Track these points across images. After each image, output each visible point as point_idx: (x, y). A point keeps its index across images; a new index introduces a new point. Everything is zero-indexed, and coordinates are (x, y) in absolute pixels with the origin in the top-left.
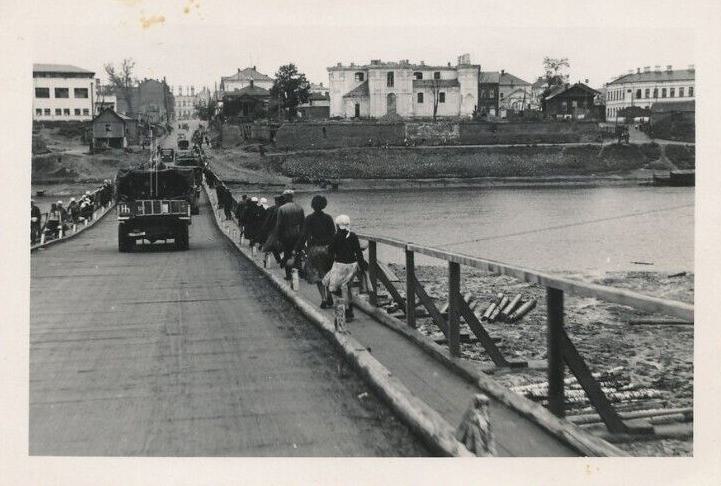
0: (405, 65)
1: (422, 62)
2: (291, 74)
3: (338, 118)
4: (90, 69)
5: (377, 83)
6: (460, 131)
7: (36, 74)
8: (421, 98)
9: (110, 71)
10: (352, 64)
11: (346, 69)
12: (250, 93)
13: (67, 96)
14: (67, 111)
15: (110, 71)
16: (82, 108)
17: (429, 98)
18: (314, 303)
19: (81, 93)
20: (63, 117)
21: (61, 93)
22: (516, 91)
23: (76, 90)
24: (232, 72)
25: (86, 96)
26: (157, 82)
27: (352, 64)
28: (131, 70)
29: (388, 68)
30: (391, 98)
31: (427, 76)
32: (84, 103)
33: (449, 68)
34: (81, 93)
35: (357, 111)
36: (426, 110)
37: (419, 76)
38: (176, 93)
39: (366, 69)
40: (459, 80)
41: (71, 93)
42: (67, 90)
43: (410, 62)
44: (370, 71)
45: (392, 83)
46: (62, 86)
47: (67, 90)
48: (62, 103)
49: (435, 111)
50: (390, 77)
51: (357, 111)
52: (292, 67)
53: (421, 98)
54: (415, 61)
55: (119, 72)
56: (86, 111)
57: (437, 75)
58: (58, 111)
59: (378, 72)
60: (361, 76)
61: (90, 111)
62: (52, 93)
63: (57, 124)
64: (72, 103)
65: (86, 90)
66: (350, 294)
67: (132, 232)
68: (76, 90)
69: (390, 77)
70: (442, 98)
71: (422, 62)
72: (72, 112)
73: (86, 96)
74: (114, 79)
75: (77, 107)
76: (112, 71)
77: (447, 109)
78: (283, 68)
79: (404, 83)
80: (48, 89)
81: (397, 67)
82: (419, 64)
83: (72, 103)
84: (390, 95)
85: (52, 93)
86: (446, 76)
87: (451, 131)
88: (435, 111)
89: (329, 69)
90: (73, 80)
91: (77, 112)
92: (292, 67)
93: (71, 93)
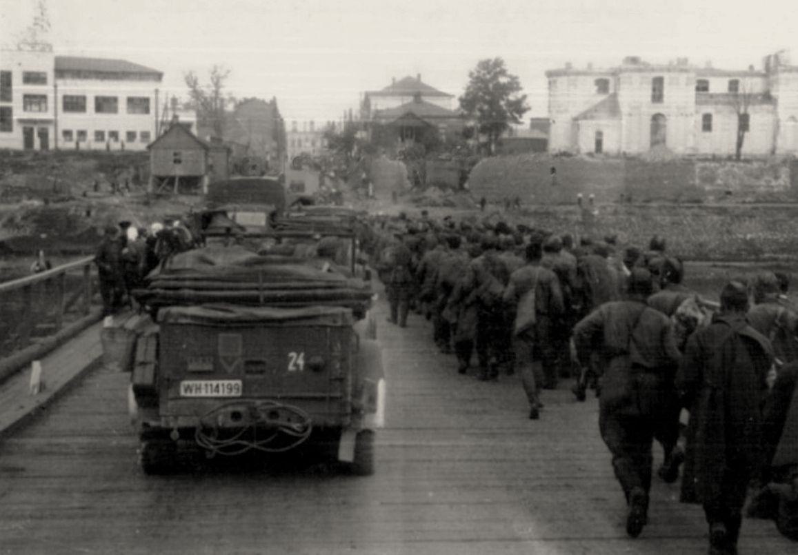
0: (681, 67)
3: (565, 154)
4: (158, 68)
5: (634, 94)
7: (46, 31)
8: (707, 124)
9: (192, 82)
10: (590, 66)
11: (578, 74)
14: (114, 135)
15: (192, 82)
16: (138, 130)
17: (725, 124)
18: (71, 270)
19: (139, 105)
21: (105, 104)
24: (380, 83)
25: (147, 111)
26: (263, 102)
27: (590, 66)
28: (223, 82)
29: (653, 70)
31: (718, 86)
33: (751, 73)
34: (139, 105)
35: (599, 143)
36: (722, 139)
37: (702, 87)
38: (288, 127)
39: (615, 73)
40: (773, 93)
41: (122, 105)
42: (115, 100)
44: (623, 76)
46: (107, 94)
47: (115, 100)
48: (106, 122)
49: (740, 144)
50: (658, 85)
51: (599, 143)
53: (707, 124)
54: (697, 59)
57: (734, 85)
58: (100, 135)
59: (636, 77)
60: (602, 85)
62: (91, 105)
65: (146, 100)
67: (780, 359)
69: (658, 85)
73: (147, 111)
74: (196, 94)
75: (131, 129)
76: (195, 83)
78: (485, 65)
79: (680, 95)
80: (84, 98)
81: (669, 69)
82: (702, 66)
83: (123, 121)
85: (91, 105)
86: (752, 86)
87: (777, 178)
88: (740, 144)
89: (551, 75)
92: (498, 63)
93: (122, 105)
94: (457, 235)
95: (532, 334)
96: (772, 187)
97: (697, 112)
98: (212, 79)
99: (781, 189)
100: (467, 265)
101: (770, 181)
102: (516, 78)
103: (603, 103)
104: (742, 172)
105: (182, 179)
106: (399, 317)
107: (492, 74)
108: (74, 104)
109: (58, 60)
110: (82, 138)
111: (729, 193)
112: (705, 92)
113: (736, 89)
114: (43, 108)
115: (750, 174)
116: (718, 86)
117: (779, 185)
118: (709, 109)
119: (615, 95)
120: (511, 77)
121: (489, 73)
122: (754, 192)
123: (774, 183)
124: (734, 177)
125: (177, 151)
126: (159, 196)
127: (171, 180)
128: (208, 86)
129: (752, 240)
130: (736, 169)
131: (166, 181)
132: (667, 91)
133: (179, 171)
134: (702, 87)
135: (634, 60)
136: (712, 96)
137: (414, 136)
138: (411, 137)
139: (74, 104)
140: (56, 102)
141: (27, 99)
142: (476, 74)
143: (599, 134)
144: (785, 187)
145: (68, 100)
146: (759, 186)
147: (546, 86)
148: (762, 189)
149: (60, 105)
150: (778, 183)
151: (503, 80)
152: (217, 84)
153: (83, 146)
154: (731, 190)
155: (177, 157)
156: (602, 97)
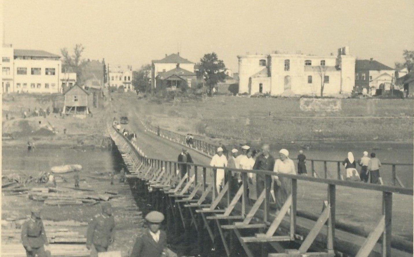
1: (214, 166)
2: (213, 61)
6: (343, 105)
12: (177, 73)
13: (40, 74)
17: (317, 80)
20: (36, 90)
22: (382, 75)
23: (25, 73)
25: (54, 74)
30: (287, 79)
32: (51, 79)
35: (261, 88)
36: (314, 89)
43: (181, 55)
45: (288, 68)
51: (261, 88)
52: (214, 55)
55: (71, 54)
56: (53, 85)
58: (33, 85)
61: (57, 85)
63: (34, 95)
64: (42, 78)
66: (265, 223)
68: (25, 73)
70: (327, 79)
71: (214, 166)
72: (43, 86)
76: (67, 54)
77: (331, 89)
78: (207, 56)
84: (286, 77)
87: (335, 105)
90: (45, 60)
91: (47, 86)
92: (214, 55)
96: (334, 109)
98: (75, 52)
100: (325, 196)
101: (333, 107)
104: (320, 103)
105: (77, 107)
107: (211, 60)
108: (21, 71)
109: (15, 51)
110: (25, 86)
112: (310, 66)
113: (324, 64)
114: (8, 73)
115: (324, 104)
116: (315, 62)
117: (336, 109)
120: (220, 61)
121: (209, 59)
122: (326, 112)
123: (334, 108)
125: (76, 96)
126: (67, 115)
127: (73, 108)
128: (74, 57)
130: (317, 102)
131: (71, 109)
133: (77, 104)
137: (176, 85)
138: (175, 85)
139: (21, 71)
140: (14, 71)
141: (4, 69)
143: (261, 85)
145: (19, 69)
146: (328, 109)
148: (329, 110)
149: (16, 72)
150: (336, 108)
151: (216, 63)
152: (78, 55)
153: (25, 90)
155: (76, 98)
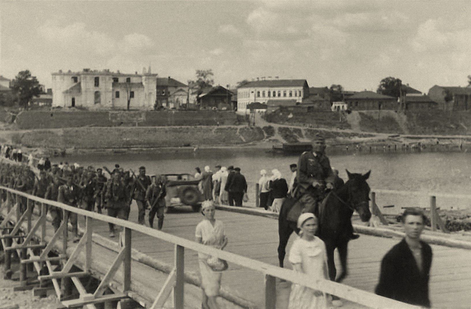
0: (107, 73)
31: (121, 80)
37: (116, 80)
59: (88, 77)
60: (75, 79)
78: (21, 73)
79: (106, 85)
82: (115, 72)
87: (141, 117)
94: (41, 255)
95: (386, 81)
97: (113, 90)
99: (142, 121)
102: (35, 77)
103: (75, 86)
106: (147, 218)
111: (122, 123)
117: (141, 120)
118: (118, 89)
119: (80, 83)
124: (124, 117)
129: (129, 141)
130: (125, 114)
132: (100, 82)
134: (116, 80)
135: (86, 70)
136: (120, 84)
142: (18, 77)
144: (144, 120)
146: (134, 120)
147: (52, 78)
154: (123, 122)
156: (75, 84)
